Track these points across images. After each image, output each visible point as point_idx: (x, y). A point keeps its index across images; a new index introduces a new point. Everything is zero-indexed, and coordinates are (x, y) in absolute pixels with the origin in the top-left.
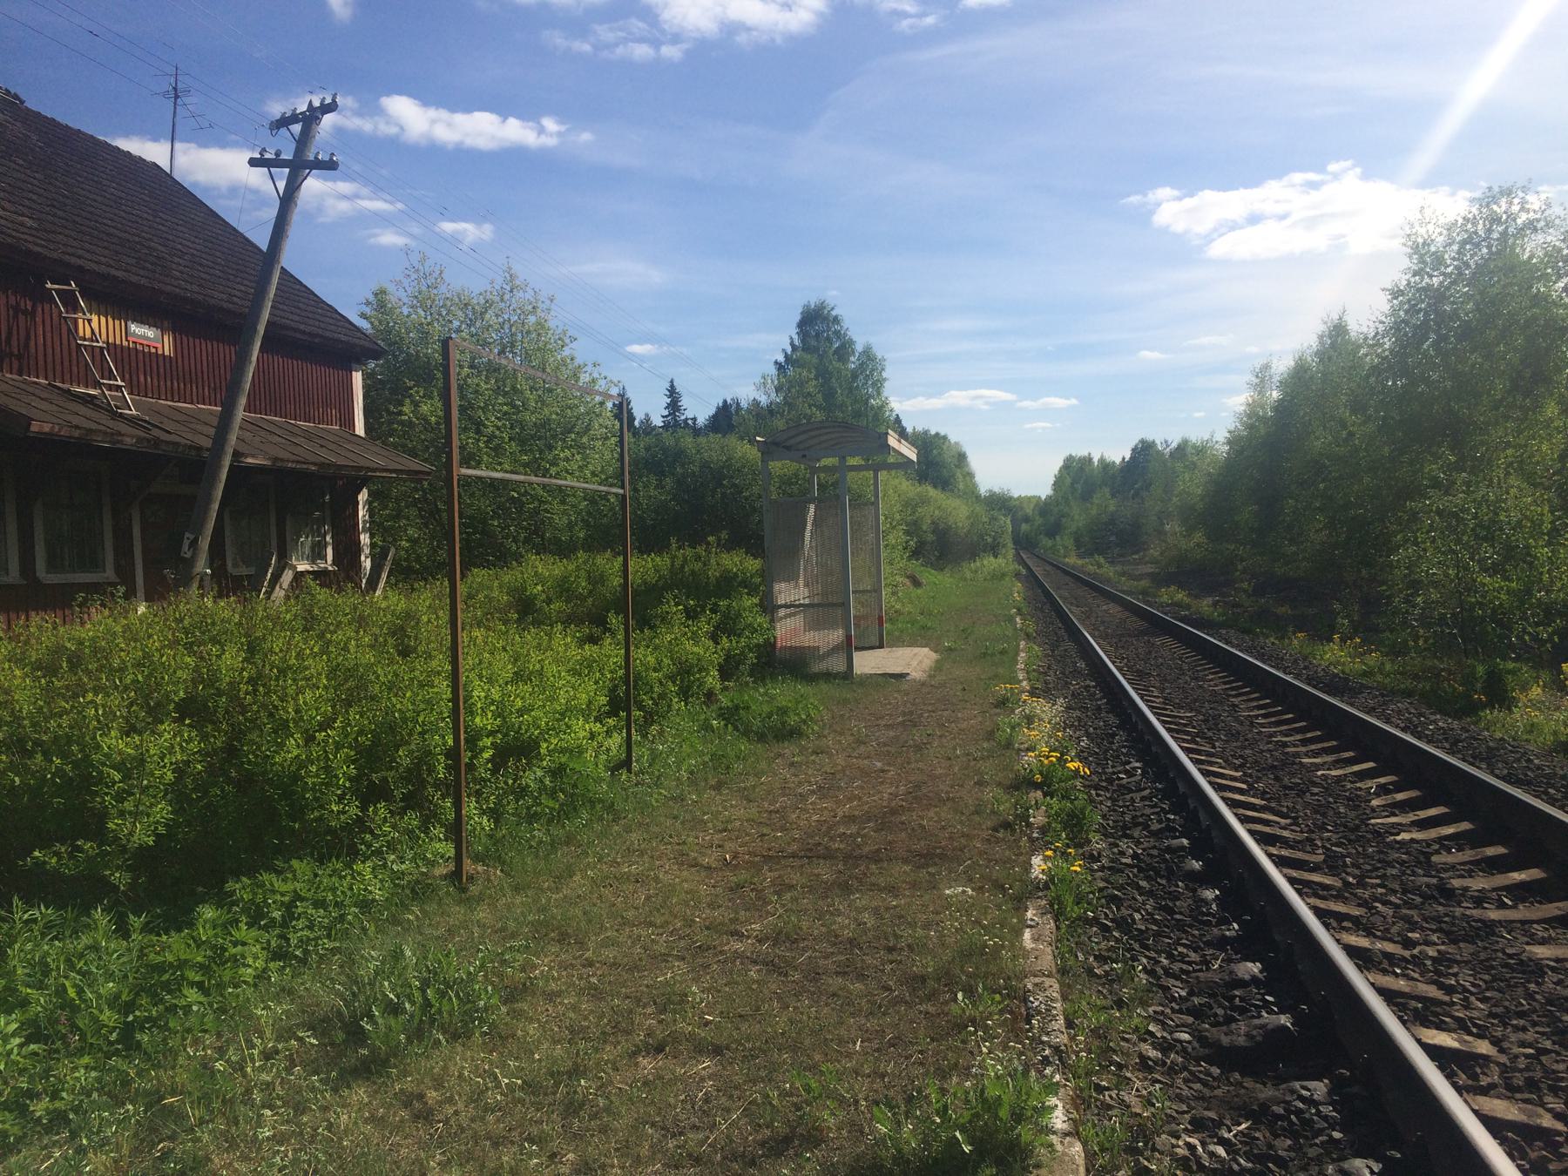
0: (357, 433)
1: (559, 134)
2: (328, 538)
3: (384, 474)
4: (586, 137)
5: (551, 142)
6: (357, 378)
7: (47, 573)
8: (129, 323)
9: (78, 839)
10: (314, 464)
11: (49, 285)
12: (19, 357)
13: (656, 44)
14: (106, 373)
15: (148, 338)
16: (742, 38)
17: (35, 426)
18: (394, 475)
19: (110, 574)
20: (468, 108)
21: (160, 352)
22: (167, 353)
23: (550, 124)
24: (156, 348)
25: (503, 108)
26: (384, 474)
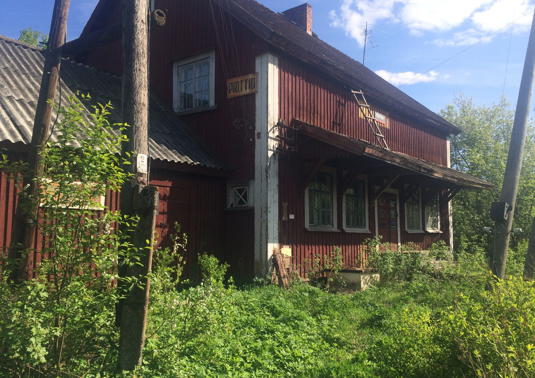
0: (448, 167)
1: (436, 76)
2: (439, 217)
3: (478, 186)
4: (447, 76)
5: (432, 79)
6: (448, 143)
7: (346, 227)
8: (376, 112)
9: (132, 266)
10: (457, 179)
11: (353, 91)
12: (340, 125)
13: (480, 37)
14: (376, 131)
15: (381, 120)
16: (516, 30)
17: (367, 150)
18: (481, 187)
19: (367, 230)
20: (403, 71)
21: (385, 127)
22: (387, 128)
23: (432, 73)
24: (384, 124)
25: (415, 69)
26: (478, 186)
